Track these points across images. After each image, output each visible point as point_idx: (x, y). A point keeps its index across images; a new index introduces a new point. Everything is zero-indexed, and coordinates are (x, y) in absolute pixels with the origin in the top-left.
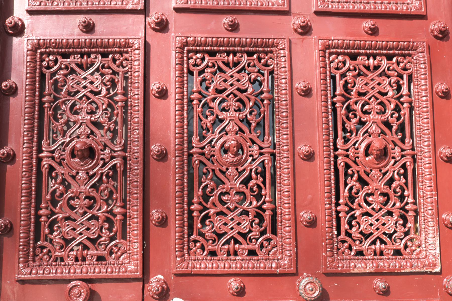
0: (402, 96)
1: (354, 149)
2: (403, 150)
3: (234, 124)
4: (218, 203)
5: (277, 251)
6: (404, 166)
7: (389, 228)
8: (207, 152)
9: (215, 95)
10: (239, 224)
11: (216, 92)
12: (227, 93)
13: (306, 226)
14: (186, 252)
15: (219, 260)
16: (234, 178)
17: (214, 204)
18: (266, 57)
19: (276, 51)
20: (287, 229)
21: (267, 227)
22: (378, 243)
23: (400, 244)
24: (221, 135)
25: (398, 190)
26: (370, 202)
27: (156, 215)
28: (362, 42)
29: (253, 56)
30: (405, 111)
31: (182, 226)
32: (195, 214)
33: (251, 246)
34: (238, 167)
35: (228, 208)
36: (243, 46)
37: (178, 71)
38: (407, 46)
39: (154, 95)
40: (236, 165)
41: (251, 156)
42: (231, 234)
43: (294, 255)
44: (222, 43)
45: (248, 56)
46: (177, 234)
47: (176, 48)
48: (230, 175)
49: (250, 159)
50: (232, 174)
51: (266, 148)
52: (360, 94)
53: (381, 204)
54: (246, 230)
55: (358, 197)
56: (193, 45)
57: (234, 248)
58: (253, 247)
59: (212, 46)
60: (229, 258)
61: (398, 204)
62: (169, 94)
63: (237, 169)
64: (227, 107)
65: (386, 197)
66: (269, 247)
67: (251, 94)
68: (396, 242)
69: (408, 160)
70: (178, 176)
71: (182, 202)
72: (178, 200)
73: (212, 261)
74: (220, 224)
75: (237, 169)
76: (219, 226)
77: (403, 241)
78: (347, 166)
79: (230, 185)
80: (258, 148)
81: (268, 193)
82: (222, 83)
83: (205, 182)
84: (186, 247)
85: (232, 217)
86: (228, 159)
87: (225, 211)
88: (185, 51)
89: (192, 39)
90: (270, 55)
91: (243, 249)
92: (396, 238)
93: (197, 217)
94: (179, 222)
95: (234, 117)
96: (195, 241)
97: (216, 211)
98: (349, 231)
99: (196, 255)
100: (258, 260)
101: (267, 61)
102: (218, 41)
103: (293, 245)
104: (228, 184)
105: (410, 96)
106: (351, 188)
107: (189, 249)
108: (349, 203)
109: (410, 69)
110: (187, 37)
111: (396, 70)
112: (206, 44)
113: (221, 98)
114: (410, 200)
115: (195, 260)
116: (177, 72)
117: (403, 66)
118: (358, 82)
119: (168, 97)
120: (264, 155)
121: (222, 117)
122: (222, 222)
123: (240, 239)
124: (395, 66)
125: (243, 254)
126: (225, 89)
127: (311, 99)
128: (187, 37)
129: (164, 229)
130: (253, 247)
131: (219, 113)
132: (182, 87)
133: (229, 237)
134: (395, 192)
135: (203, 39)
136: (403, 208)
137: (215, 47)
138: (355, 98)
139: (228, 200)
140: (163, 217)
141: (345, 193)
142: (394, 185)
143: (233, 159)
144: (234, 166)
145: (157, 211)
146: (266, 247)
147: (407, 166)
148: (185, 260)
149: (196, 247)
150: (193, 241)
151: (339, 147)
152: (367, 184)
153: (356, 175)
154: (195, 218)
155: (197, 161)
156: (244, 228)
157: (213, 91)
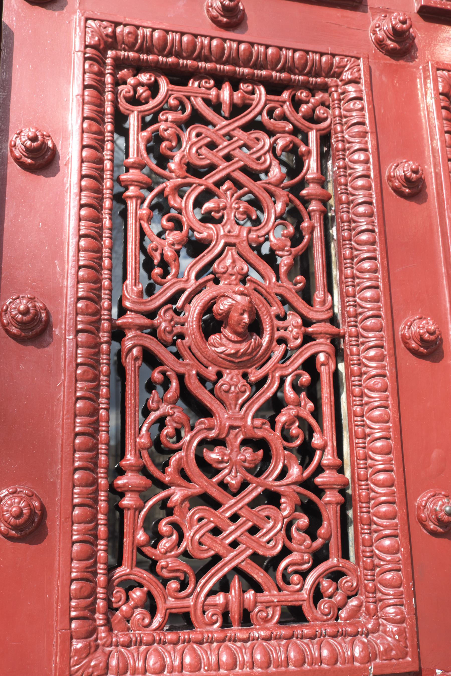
0: (303, 184)
1: (171, 313)
2: (307, 322)
3: (237, 256)
4: (193, 469)
5: (360, 606)
6: (310, 365)
7: (268, 542)
8: (163, 325)
9: (185, 177)
10: (254, 530)
11: (188, 171)
12: (217, 177)
13: (433, 533)
14: (100, 618)
15: (200, 643)
16: (238, 399)
17: (183, 474)
18: (312, 100)
19: (337, 86)
20: (387, 542)
21: (329, 539)
22: (236, 583)
23: (301, 589)
24: (201, 281)
25: (294, 430)
26: (215, 465)
27: (11, 505)
28: (297, 55)
29: (279, 93)
30: (312, 224)
31: (91, 540)
32: (127, 501)
33: (288, 596)
34: (249, 370)
35: (223, 485)
36: (256, 66)
37: (88, 103)
38: (190, 48)
39: (18, 160)
40: (242, 362)
41: (282, 341)
42: (232, 559)
43: (411, 618)
44: (206, 51)
45: (268, 92)
46: (75, 564)
47: (86, 46)
48: (227, 392)
49: (279, 351)
50: (233, 388)
51: (319, 321)
52: (194, 170)
53: (248, 470)
54: (275, 547)
55: (180, 449)
56: (131, 48)
57: (241, 601)
58: (296, 596)
59: (179, 55)
60: (230, 633)
61: (295, 471)
62: (61, 163)
63: (245, 376)
64: (218, 212)
65: (261, 452)
66: (338, 598)
67: (278, 184)
68: (289, 584)
69: (321, 350)
70: (82, 389)
71: (92, 466)
72: (80, 459)
73: (180, 646)
74: (202, 532)
75: (245, 376)
76: (197, 537)
77: (310, 580)
78: (150, 359)
79: (229, 418)
80: (300, 321)
81: (329, 443)
82: (204, 151)
83: (158, 409)
84: (101, 604)
85: (235, 509)
86: (222, 345)
87: (216, 493)
88: (108, 61)
89: (127, 30)
90: (319, 96)
91: (268, 604)
92: (290, 570)
93: (136, 509)
94: (82, 526)
95: (238, 236)
96: (129, 586)
97: (190, 492)
98: (148, 550)
99: (128, 629)
100: (312, 638)
101: (314, 110)
102: (165, 40)
103: (408, 588)
104: (223, 417)
105: (323, 183)
106: (161, 422)
107: (111, 609)
108: (153, 469)
109: (325, 119)
110: (117, 24)
111: (292, 119)
112: (163, 48)
113: (203, 187)
114: (328, 458)
115: (127, 645)
116: (86, 107)
117: (306, 111)
118: (189, 139)
119: (58, 170)
120: (314, 340)
121: (205, 234)
122: (206, 524)
123: (259, 575)
124: (287, 107)
125: (266, 620)
126: (212, 167)
127: (424, 205)
128: (117, 24)
129: (34, 547)
130: (296, 596)
131: (197, 225)
132: (98, 146)
133: (226, 569)
134: (286, 437)
135: (156, 34)
136: (308, 484)
137: (187, 58)
138: (178, 177)
139: (222, 462)
140: (32, 511)
141: (141, 435)
142: (282, 418)
143: (238, 346)
144: (239, 365)
145: (14, 493)
146: (331, 597)
147: (318, 366)
148: (97, 646)
149: (132, 603)
150: (120, 584)
151: (128, 304)
152: (204, 412)
153: (174, 384)
154: (128, 515)
155: (135, 351)
156: (268, 542)
157: (182, 168)
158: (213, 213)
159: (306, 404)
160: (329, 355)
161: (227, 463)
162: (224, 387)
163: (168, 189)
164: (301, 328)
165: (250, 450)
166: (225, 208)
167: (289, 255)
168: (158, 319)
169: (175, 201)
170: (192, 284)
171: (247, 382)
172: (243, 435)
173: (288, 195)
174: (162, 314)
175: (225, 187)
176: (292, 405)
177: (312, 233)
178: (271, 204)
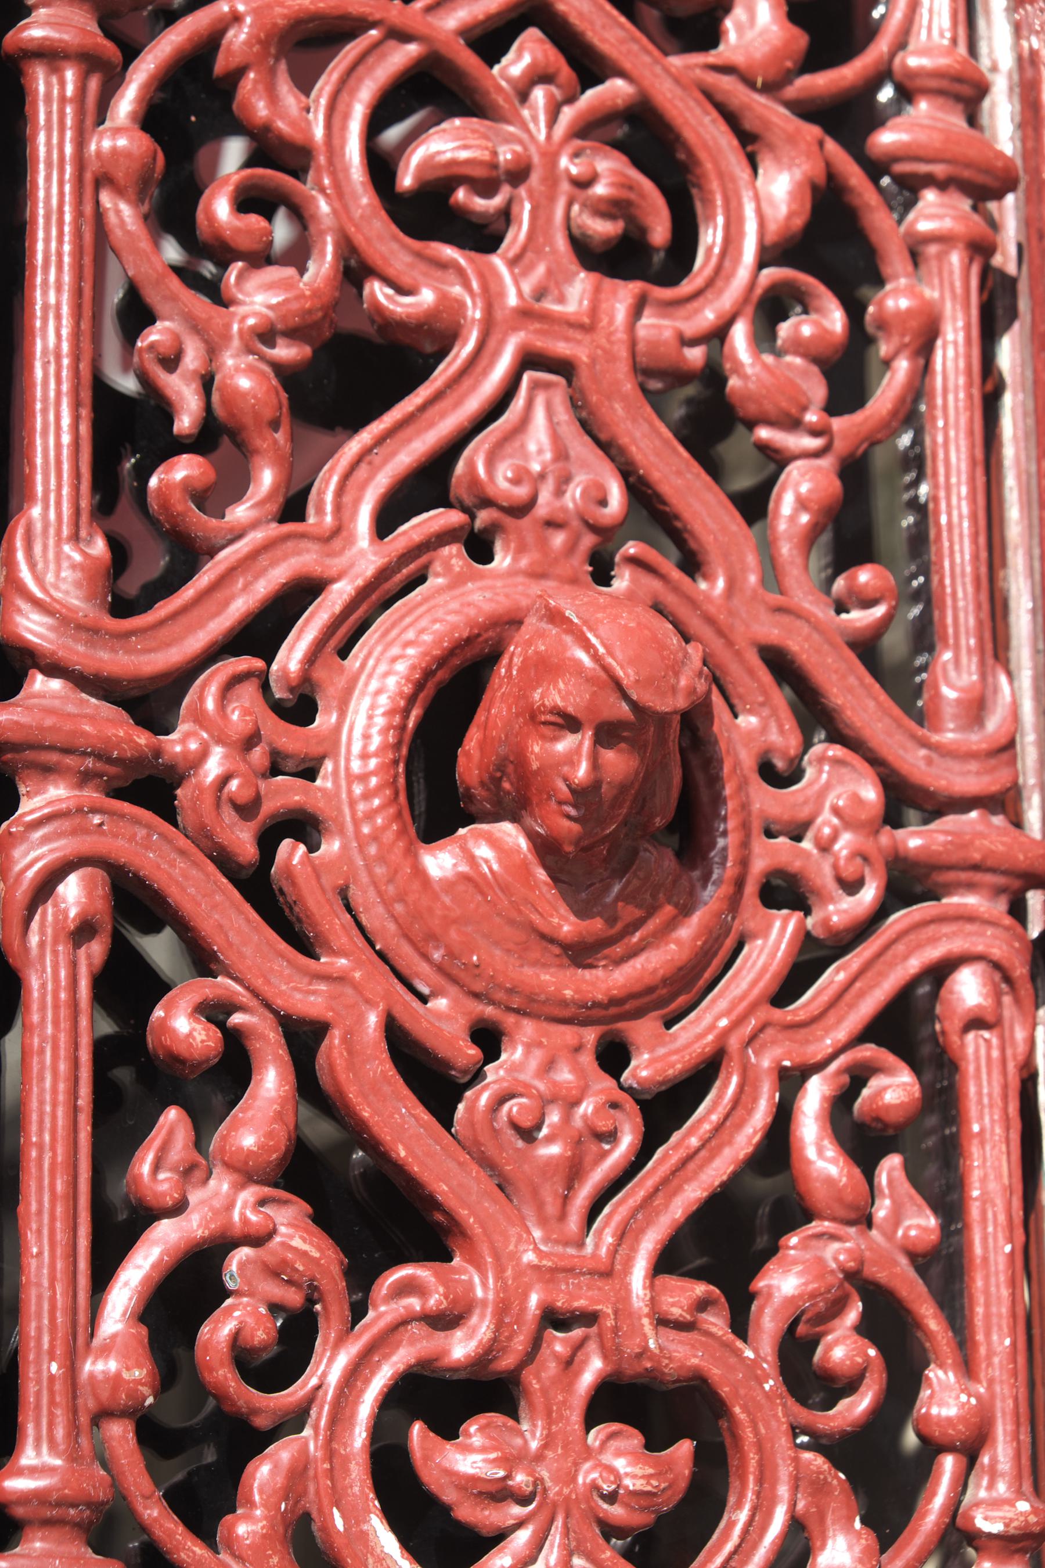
2: (903, 799)
6: (906, 1026)
8: (213, 767)
25: (841, 1347)
41: (785, 892)
50: (554, 1117)
64: (487, 187)
75: (613, 1057)
80: (870, 793)
95: (586, 326)
106: (188, 1291)
113: (413, 49)
142: (784, 1283)
155: (72, 891)
158: (461, 194)
159: (896, 1217)
160: (1007, 979)
161: (524, 1501)
162: (512, 1107)
163: (238, 37)
164: (877, 832)
165: (634, 1439)
166: (518, 175)
167: (817, 454)
168: (187, 736)
169: (273, 99)
170: (364, 555)
171: (621, 1087)
172: (605, 1357)
173: (821, 144)
174: (210, 704)
175: (516, 63)
176: (833, 1219)
177: (924, 346)
178: (743, 173)
